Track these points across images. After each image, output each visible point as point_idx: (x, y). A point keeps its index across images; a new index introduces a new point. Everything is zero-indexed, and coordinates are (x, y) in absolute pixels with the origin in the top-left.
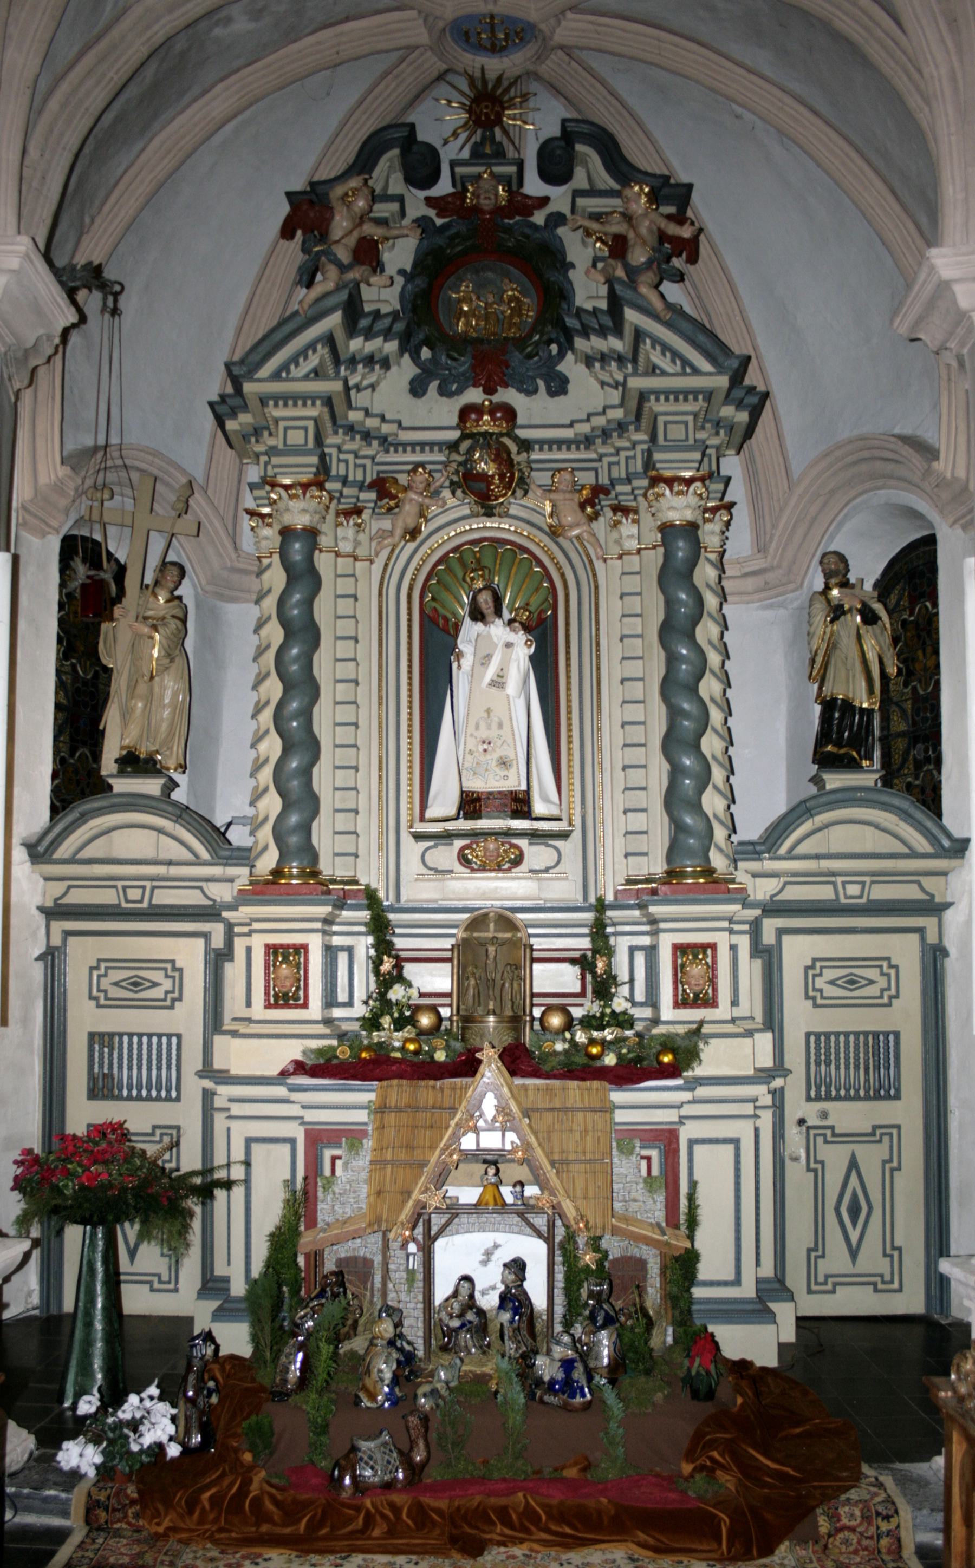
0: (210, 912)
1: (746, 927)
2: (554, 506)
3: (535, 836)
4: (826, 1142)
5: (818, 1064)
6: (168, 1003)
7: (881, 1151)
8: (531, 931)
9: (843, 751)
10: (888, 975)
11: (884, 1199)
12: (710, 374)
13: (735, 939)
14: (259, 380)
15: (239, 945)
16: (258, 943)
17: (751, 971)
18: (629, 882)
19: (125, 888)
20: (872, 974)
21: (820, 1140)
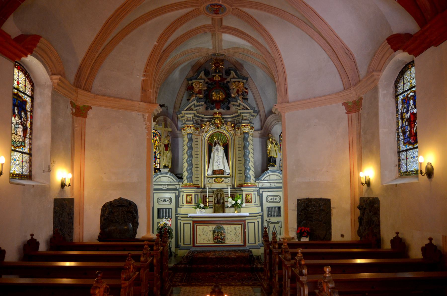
0: (176, 190)
1: (257, 191)
2: (228, 128)
3: (225, 177)
4: (270, 224)
5: (268, 212)
6: (170, 203)
7: (279, 225)
8: (224, 192)
9: (273, 164)
10: (279, 198)
11: (279, 233)
12: (250, 110)
13: (255, 193)
14: (184, 111)
15: (181, 194)
16: (185, 194)
17: (258, 198)
18: (239, 184)
19: (163, 186)
20: (277, 198)
21: (269, 223)
